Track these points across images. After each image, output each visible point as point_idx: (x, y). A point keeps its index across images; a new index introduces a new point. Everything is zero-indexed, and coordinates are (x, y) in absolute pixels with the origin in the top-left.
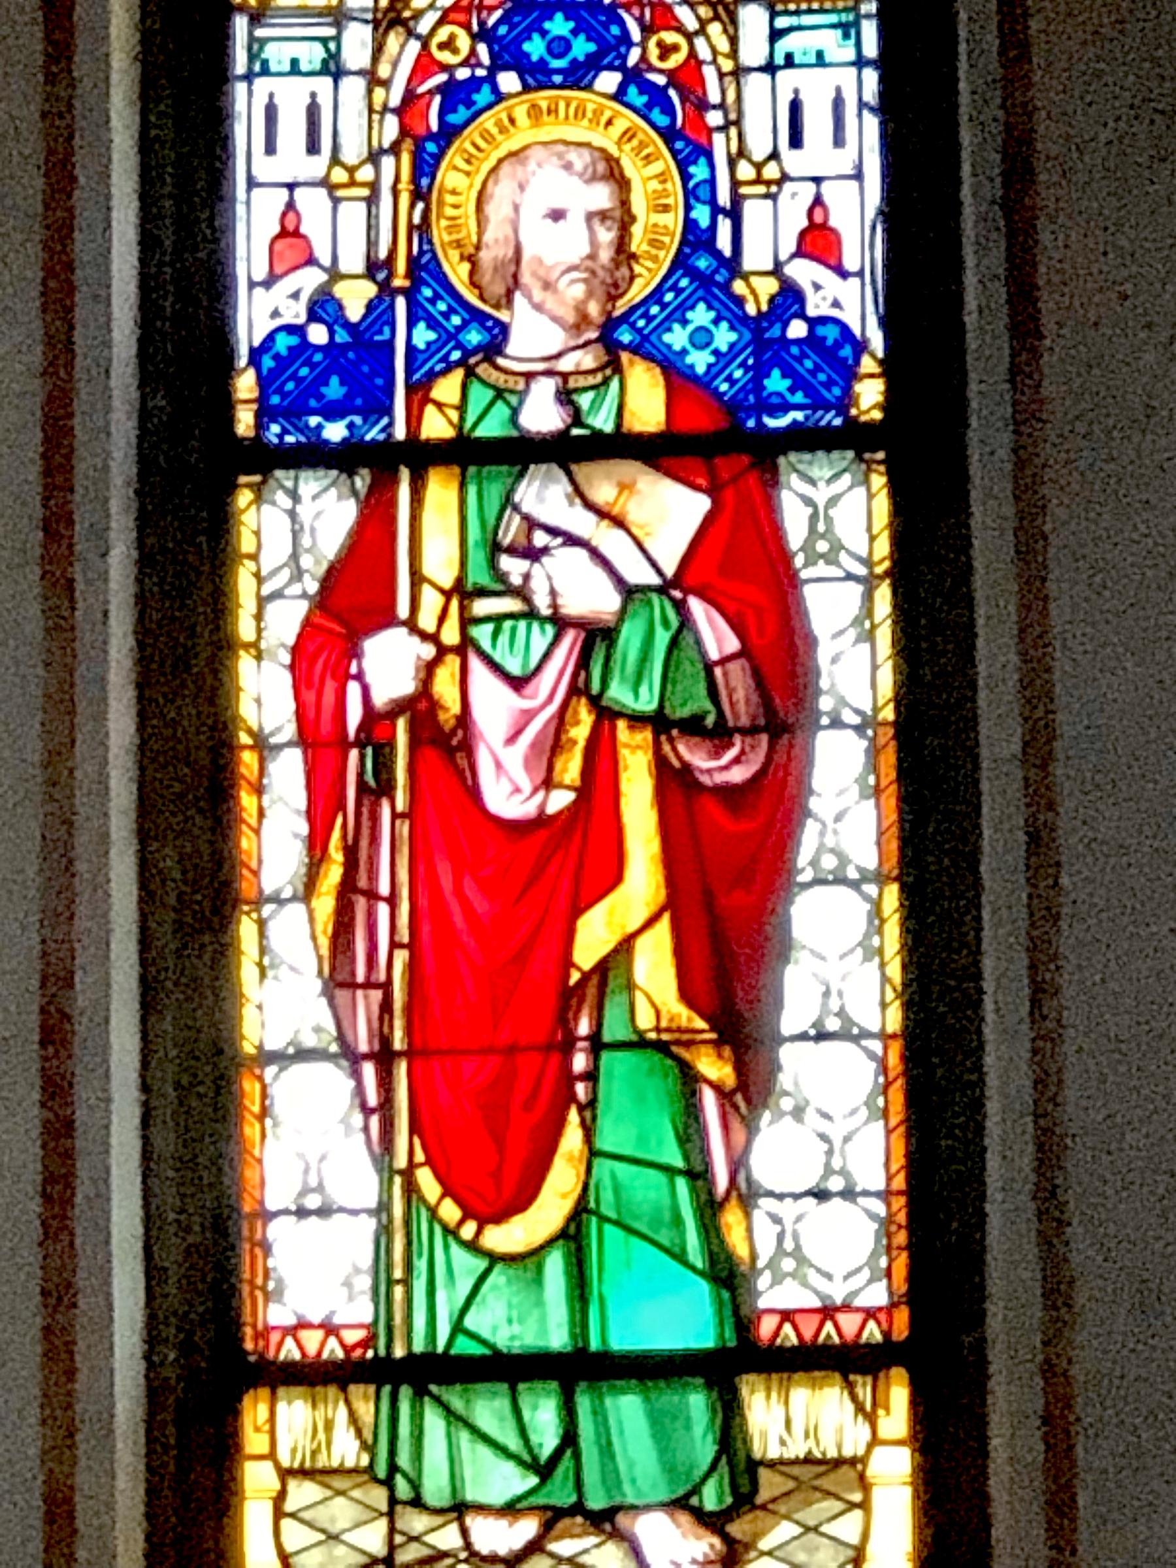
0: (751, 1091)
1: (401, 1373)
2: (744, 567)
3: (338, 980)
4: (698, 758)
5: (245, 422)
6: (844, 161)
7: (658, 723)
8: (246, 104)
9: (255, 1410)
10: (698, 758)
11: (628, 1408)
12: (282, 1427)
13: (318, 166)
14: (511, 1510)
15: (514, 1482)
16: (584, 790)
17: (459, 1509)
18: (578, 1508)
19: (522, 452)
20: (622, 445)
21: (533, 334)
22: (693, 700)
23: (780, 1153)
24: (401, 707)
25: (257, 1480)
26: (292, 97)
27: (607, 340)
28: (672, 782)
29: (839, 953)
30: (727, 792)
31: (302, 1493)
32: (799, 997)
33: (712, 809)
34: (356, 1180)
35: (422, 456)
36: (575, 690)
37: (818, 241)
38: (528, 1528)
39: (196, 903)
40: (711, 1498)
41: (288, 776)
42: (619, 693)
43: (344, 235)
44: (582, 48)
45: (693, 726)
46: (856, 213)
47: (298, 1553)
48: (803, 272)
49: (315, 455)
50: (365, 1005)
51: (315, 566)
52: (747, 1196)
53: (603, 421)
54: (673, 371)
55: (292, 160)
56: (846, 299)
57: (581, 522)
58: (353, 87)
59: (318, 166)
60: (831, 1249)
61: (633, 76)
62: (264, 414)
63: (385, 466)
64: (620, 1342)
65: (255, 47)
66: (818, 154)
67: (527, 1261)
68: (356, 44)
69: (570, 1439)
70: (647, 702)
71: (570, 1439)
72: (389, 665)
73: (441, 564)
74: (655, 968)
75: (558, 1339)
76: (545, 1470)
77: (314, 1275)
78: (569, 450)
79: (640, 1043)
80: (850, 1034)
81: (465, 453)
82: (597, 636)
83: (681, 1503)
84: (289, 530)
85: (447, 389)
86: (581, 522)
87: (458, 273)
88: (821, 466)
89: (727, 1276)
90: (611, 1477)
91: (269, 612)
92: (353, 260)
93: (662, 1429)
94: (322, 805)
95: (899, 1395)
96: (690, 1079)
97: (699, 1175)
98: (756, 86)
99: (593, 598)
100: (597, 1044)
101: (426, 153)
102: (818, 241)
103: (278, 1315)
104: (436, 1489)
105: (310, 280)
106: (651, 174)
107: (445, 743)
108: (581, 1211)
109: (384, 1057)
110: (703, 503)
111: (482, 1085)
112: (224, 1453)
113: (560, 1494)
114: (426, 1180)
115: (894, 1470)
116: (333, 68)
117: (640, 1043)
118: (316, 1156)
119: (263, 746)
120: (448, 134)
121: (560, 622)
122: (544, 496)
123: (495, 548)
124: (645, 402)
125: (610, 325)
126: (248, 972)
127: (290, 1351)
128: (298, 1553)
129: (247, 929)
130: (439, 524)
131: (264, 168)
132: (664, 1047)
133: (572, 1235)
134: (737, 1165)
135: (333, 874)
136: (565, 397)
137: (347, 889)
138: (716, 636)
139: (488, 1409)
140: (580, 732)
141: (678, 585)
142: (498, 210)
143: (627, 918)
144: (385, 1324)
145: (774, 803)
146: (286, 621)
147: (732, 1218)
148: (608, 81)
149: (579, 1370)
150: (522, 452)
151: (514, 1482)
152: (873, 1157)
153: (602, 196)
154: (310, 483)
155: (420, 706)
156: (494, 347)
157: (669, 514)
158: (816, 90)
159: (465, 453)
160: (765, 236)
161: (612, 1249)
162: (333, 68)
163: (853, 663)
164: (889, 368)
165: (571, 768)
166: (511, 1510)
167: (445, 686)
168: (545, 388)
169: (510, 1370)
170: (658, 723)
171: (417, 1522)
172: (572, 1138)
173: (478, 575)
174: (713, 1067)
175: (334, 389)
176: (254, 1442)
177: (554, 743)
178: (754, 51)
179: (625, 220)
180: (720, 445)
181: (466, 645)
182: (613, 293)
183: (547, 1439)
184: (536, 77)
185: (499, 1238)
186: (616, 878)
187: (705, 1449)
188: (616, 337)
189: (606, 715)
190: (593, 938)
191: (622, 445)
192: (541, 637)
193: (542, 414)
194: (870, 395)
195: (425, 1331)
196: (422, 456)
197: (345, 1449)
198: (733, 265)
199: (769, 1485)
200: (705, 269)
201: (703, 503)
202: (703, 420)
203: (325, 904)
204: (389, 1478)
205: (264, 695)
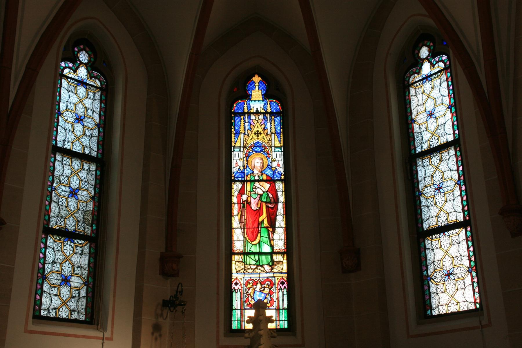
0: (274, 232)
1: (245, 253)
2: (273, 190)
3: (240, 222)
4: (269, 205)
5: (233, 178)
6: (280, 159)
7: (266, 202)
8: (233, 153)
9: (233, 257)
10: (269, 205)
11: (263, 257)
12: (236, 258)
13: (239, 158)
14: (254, 265)
15: (254, 263)
16: (260, 208)
17: (250, 265)
18: (260, 265)
19: (255, 181)
20: (263, 180)
21: (256, 172)
22: (269, 200)
23: (276, 237)
24: (245, 201)
25: (233, 262)
26: (237, 153)
27: (262, 172)
28: (267, 207)
29: (280, 221)
30: (271, 208)
31: (237, 263)
32: (277, 225)
33: (270, 209)
34: (242, 238)
35: (247, 181)
36: (259, 199)
37: (278, 165)
38: (255, 266)
39: (230, 215)
40: (270, 264)
41: (236, 206)
42: (263, 200)
43: (241, 164)
44: (260, 150)
45: (269, 203)
46: (281, 163)
47: (82, 157)
48: (277, 167)
49: (238, 181)
50: (242, 224)
51: (238, 189)
52: (273, 240)
53: (261, 179)
54: (267, 175)
55: (237, 158)
56: (281, 170)
57: (260, 187)
58: (242, 152)
59: (239, 158)
60: (280, 245)
61: (264, 152)
62: (235, 177)
63: (244, 182)
64: (263, 251)
65: (234, 149)
66: (278, 158)
67: (256, 245)
68: (242, 149)
69: (259, 259)
70: (265, 200)
71: (259, 259)
72: (244, 197)
73: (248, 189)
74: (266, 221)
75: (258, 251)
76: (257, 262)
77: (238, 246)
78: (259, 181)
79: (264, 227)
80: (282, 227)
81: (251, 181)
82: (261, 196)
83: (268, 265)
84: (237, 187)
85: (249, 176)
86: (260, 187)
87: (250, 167)
88: (279, 182)
89: (272, 246)
90: (262, 263)
91: (235, 194)
92: (242, 166)
93: (266, 258)
94: (239, 209)
95: (285, 256)
96: (268, 231)
97: (269, 238)
98: (273, 153)
99: (261, 193)
100: (261, 228)
101: (247, 157)
102: (278, 165)
103: (235, 249)
104: (248, 263)
105: (238, 167)
106: (265, 160)
107: (249, 203)
108: (260, 241)
109: (244, 228)
110: (269, 185)
111: (252, 232)
112: (231, 260)
113: (258, 264)
114: (247, 238)
115: (285, 262)
116: (240, 151)
117: (264, 227)
118: (238, 235)
119: (234, 203)
120: (249, 156)
121: (258, 194)
122: (257, 184)
123: (253, 188)
124: (265, 178)
125: (262, 171)
126: (233, 221)
127: (236, 252)
128: (82, 157)
129: (233, 218)
130: (248, 187)
131: (235, 158)
132: (267, 228)
133: (259, 243)
134: (273, 237)
135: (240, 214)
136: (258, 177)
137: (241, 215)
138: (271, 196)
139: (252, 256)
140: (260, 203)
141: (267, 192)
142: (253, 162)
143: (264, 217)
144: (244, 250)
145: (276, 208)
146: (236, 194)
147: (272, 242)
148: (262, 152)
149: (260, 254)
150: (255, 181)
151: (254, 263)
152: (283, 237)
153: (261, 161)
154: (238, 183)
155: (247, 201)
156: (253, 173)
157: (267, 186)
158: (278, 153)
159: (251, 181)
160: (274, 165)
161: (262, 243)
162: (240, 151)
163: (281, 198)
164: (284, 175)
165: (259, 206)
166: (254, 265)
167: (249, 199)
168: (257, 176)
169: (254, 253)
170: (266, 202)
171: (246, 266)
172: (259, 235)
173: (251, 190)
174: (270, 230)
175: (240, 176)
176: (233, 259)
177: (258, 204)
178: (273, 150)
179: (263, 163)
180: (271, 181)
181: (251, 196)
182: (262, 169)
183: (257, 259)
184: (256, 152)
185: (253, 243)
186: (263, 214)
187: (270, 260)
188: (262, 173)
189: (262, 201)
190: (261, 219)
191: (263, 180)
192: (257, 195)
193: (257, 178)
194: (283, 177)
195: (247, 250)
196: (247, 181)
197: (241, 260)
198: (272, 167)
199: (275, 263)
200: (270, 167)
201: (269, 185)
202: (269, 179)
203: (239, 216)
204: (244, 262)
205: (235, 200)
